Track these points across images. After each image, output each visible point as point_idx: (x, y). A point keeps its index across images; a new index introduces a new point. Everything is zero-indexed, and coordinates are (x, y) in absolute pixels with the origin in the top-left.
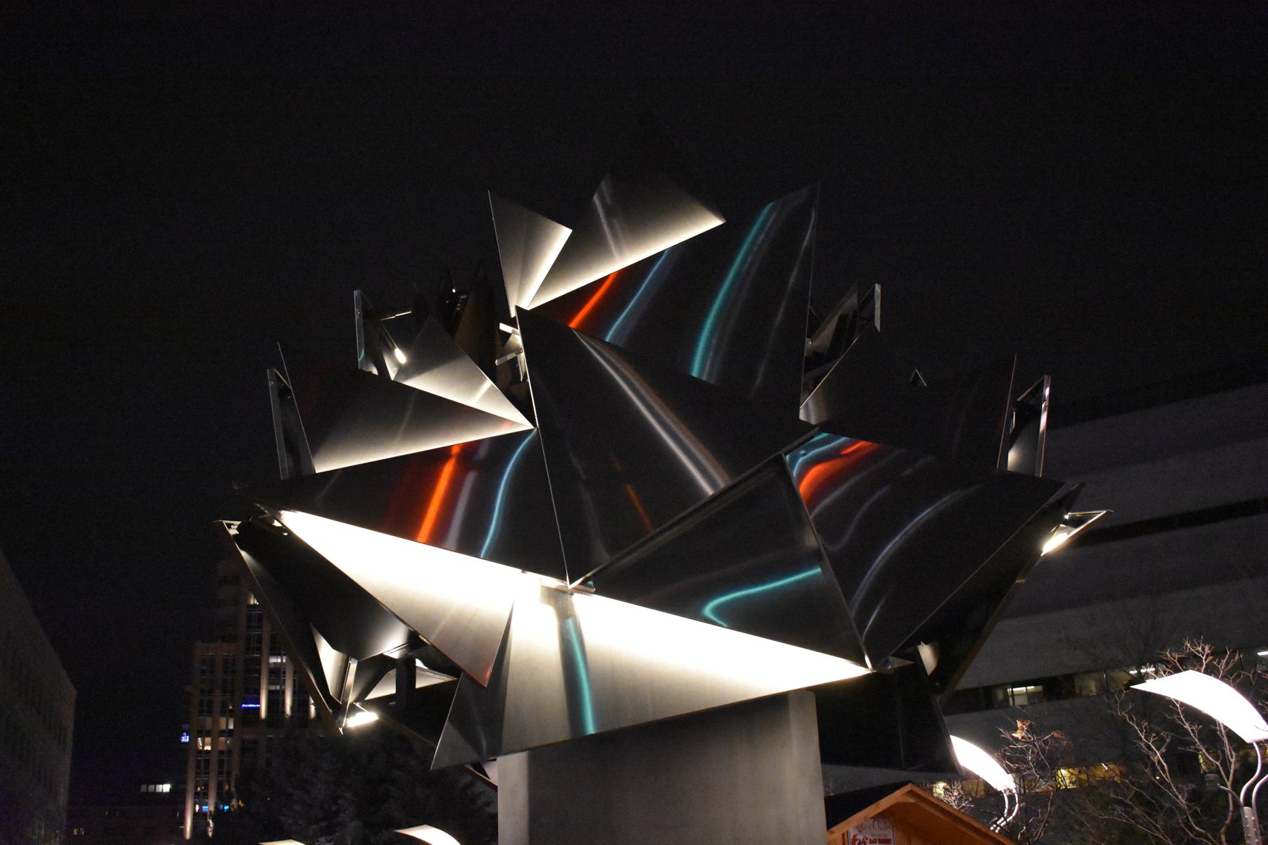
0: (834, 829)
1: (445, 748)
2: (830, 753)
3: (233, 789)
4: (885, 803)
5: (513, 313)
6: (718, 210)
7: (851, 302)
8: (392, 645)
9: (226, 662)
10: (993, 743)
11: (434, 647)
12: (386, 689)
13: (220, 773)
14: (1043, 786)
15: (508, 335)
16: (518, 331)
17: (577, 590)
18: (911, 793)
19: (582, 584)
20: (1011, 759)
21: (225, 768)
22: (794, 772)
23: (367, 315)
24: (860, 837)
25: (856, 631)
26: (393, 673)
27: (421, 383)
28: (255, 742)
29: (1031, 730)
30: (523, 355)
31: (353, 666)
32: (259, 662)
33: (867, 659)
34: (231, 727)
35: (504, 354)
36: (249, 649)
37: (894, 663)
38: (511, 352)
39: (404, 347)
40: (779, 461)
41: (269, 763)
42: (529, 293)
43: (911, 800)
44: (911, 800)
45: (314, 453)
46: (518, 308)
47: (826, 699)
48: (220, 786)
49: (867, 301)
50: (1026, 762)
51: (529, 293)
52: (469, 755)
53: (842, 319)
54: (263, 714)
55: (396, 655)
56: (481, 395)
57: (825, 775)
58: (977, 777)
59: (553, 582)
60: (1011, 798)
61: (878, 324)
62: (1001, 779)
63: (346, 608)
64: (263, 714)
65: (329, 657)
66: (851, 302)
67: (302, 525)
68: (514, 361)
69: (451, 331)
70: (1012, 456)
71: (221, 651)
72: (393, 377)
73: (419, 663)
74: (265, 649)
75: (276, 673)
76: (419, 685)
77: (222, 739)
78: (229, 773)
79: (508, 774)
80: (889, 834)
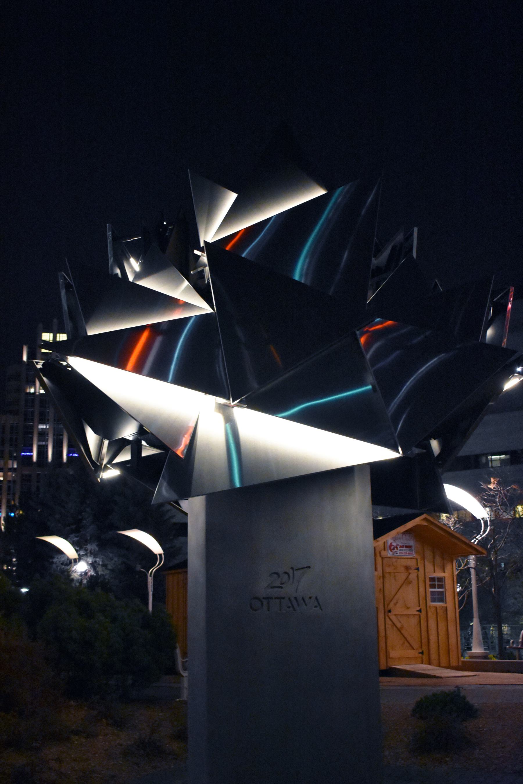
0: (378, 539)
1: (162, 491)
2: (377, 499)
3: (18, 504)
4: (410, 525)
5: (202, 244)
6: (323, 184)
7: (400, 237)
8: (129, 432)
9: (12, 428)
10: (476, 490)
11: (152, 433)
12: (125, 456)
13: (8, 494)
14: (506, 516)
15: (199, 257)
16: (205, 255)
17: (236, 405)
18: (425, 519)
19: (239, 402)
20: (486, 500)
21: (11, 492)
22: (357, 509)
23: (114, 239)
24: (394, 544)
25: (393, 429)
26: (128, 447)
27: (146, 283)
28: (30, 476)
29: (499, 483)
30: (207, 268)
31: (106, 442)
32: (32, 427)
33: (400, 449)
34: (15, 466)
35: (196, 268)
36: (26, 420)
37: (416, 451)
38: (201, 266)
39: (137, 259)
40: (354, 334)
41: (38, 488)
42: (210, 234)
43: (425, 523)
44: (425, 523)
45: (87, 322)
46: (205, 242)
47: (376, 469)
48: (8, 502)
49: (409, 237)
50: (495, 502)
51: (210, 234)
52: (173, 496)
53: (394, 248)
54: (35, 459)
55: (131, 438)
56: (181, 291)
57: (373, 509)
58: (465, 510)
59: (222, 401)
60: (486, 523)
61: (414, 255)
62: (479, 511)
63: (104, 412)
64: (35, 459)
65: (92, 437)
66: (400, 237)
67: (80, 365)
68: (203, 271)
69: (163, 250)
70: (490, 332)
71: (10, 420)
72: (131, 278)
73: (144, 443)
74: (36, 419)
75: (43, 435)
76: (144, 454)
77: (10, 473)
78: (14, 494)
79: (194, 508)
80: (412, 543)
